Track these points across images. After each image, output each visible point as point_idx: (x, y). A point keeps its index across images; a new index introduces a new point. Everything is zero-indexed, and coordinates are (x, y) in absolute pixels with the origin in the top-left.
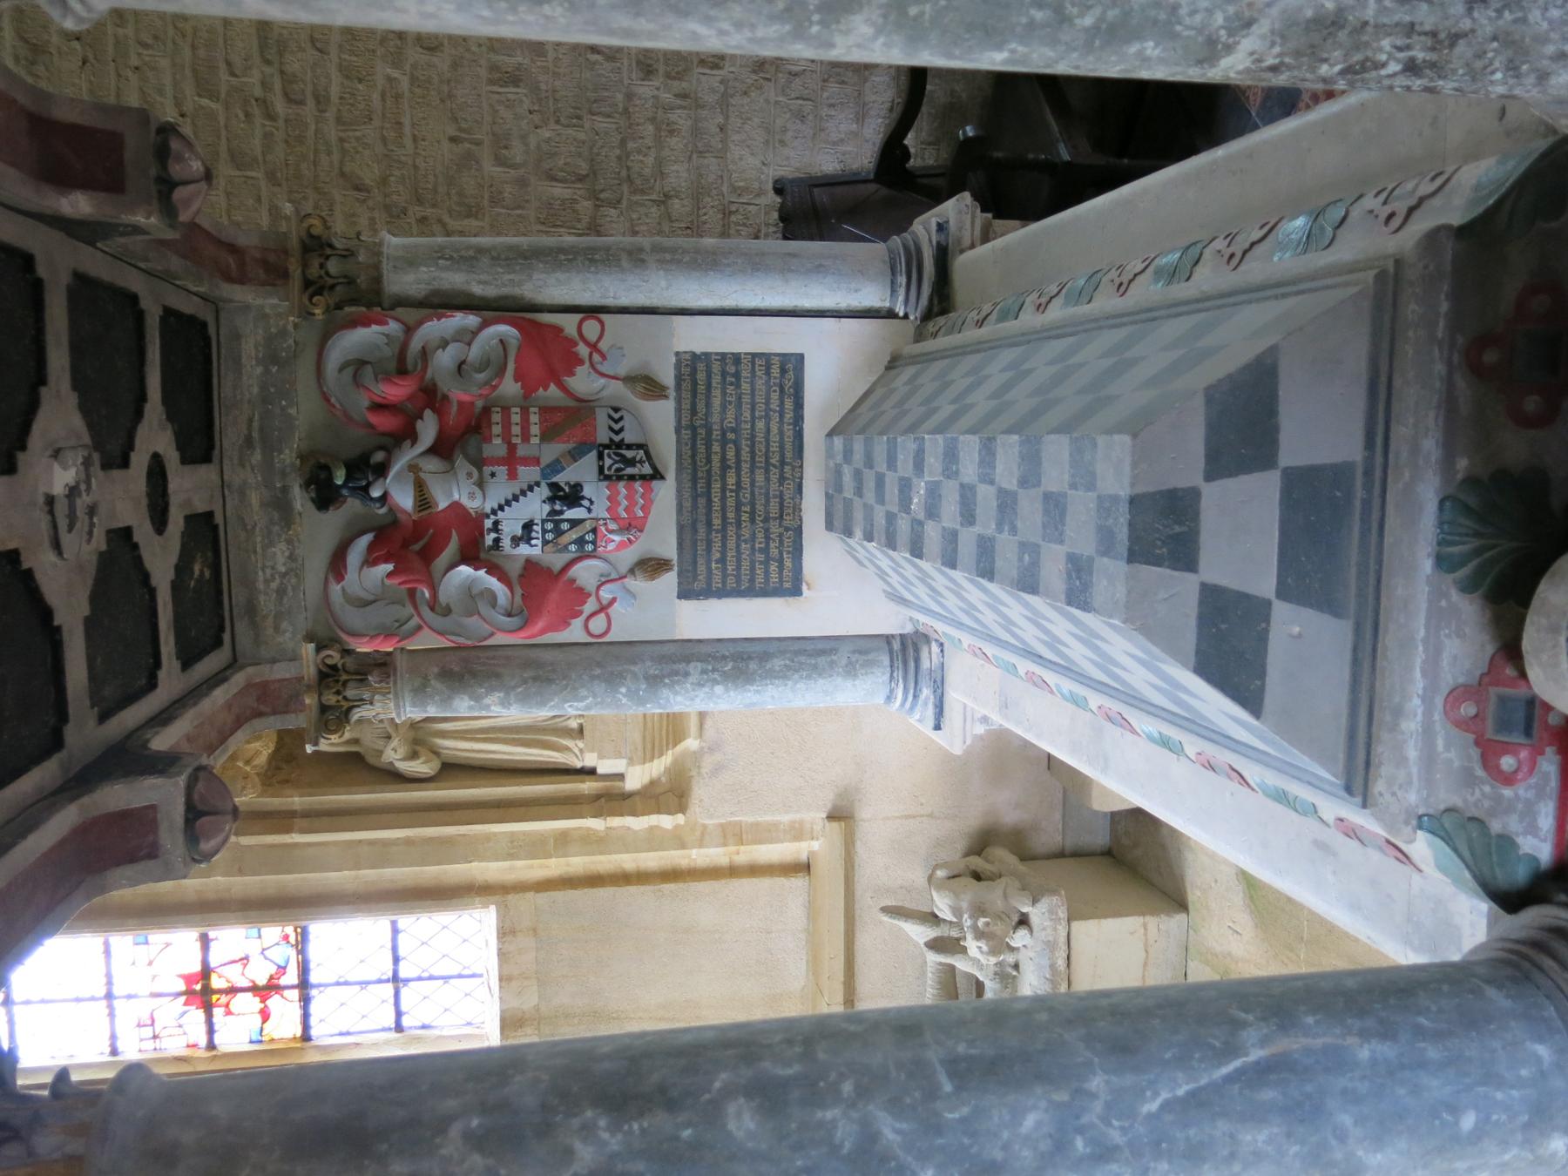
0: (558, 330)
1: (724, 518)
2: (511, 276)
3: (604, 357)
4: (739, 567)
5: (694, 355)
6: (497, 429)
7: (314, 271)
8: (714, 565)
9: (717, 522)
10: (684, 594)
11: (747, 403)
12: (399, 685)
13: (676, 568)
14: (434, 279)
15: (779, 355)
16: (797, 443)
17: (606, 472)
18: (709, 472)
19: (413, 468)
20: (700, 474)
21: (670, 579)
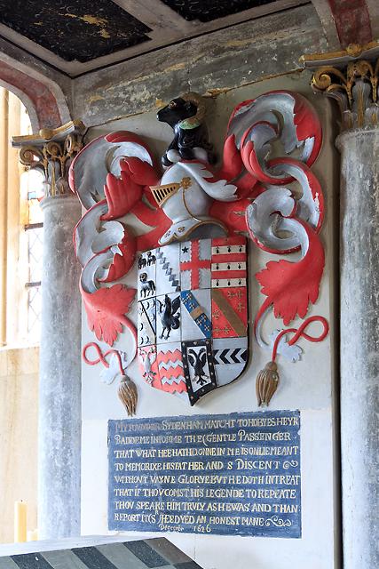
0: (314, 297)
1: (167, 460)
2: (357, 249)
3: (292, 343)
4: (130, 473)
5: (297, 428)
6: (224, 250)
7: (352, 72)
8: (132, 451)
9: (163, 453)
10: (112, 426)
11: (257, 481)
12: (54, 201)
13: (130, 418)
14: (353, 179)
15: (299, 513)
16: (224, 529)
17: (189, 349)
18: (201, 445)
19: (187, 181)
20: (199, 437)
21: (121, 413)
